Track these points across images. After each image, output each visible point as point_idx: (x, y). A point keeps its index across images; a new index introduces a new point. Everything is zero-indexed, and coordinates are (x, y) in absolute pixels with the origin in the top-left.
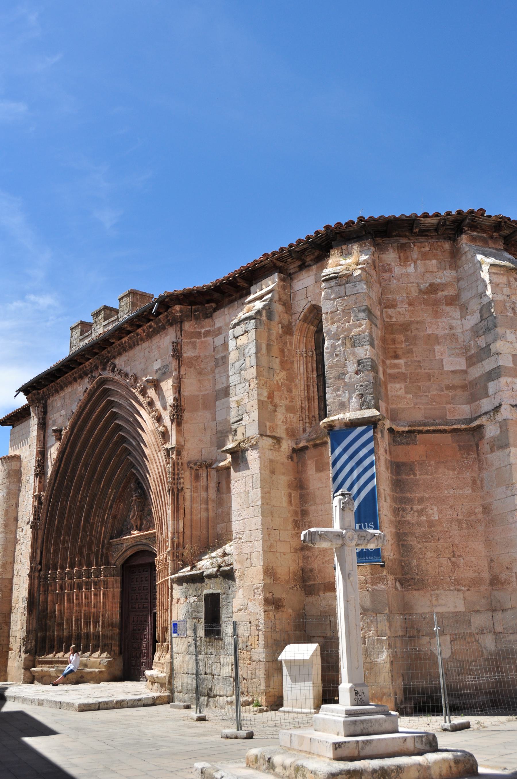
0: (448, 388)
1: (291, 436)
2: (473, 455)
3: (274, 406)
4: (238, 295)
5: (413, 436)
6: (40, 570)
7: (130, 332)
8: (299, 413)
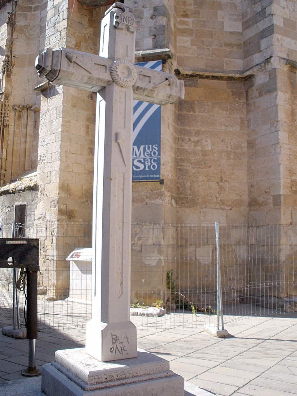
0: (227, 45)
5: (195, 79)
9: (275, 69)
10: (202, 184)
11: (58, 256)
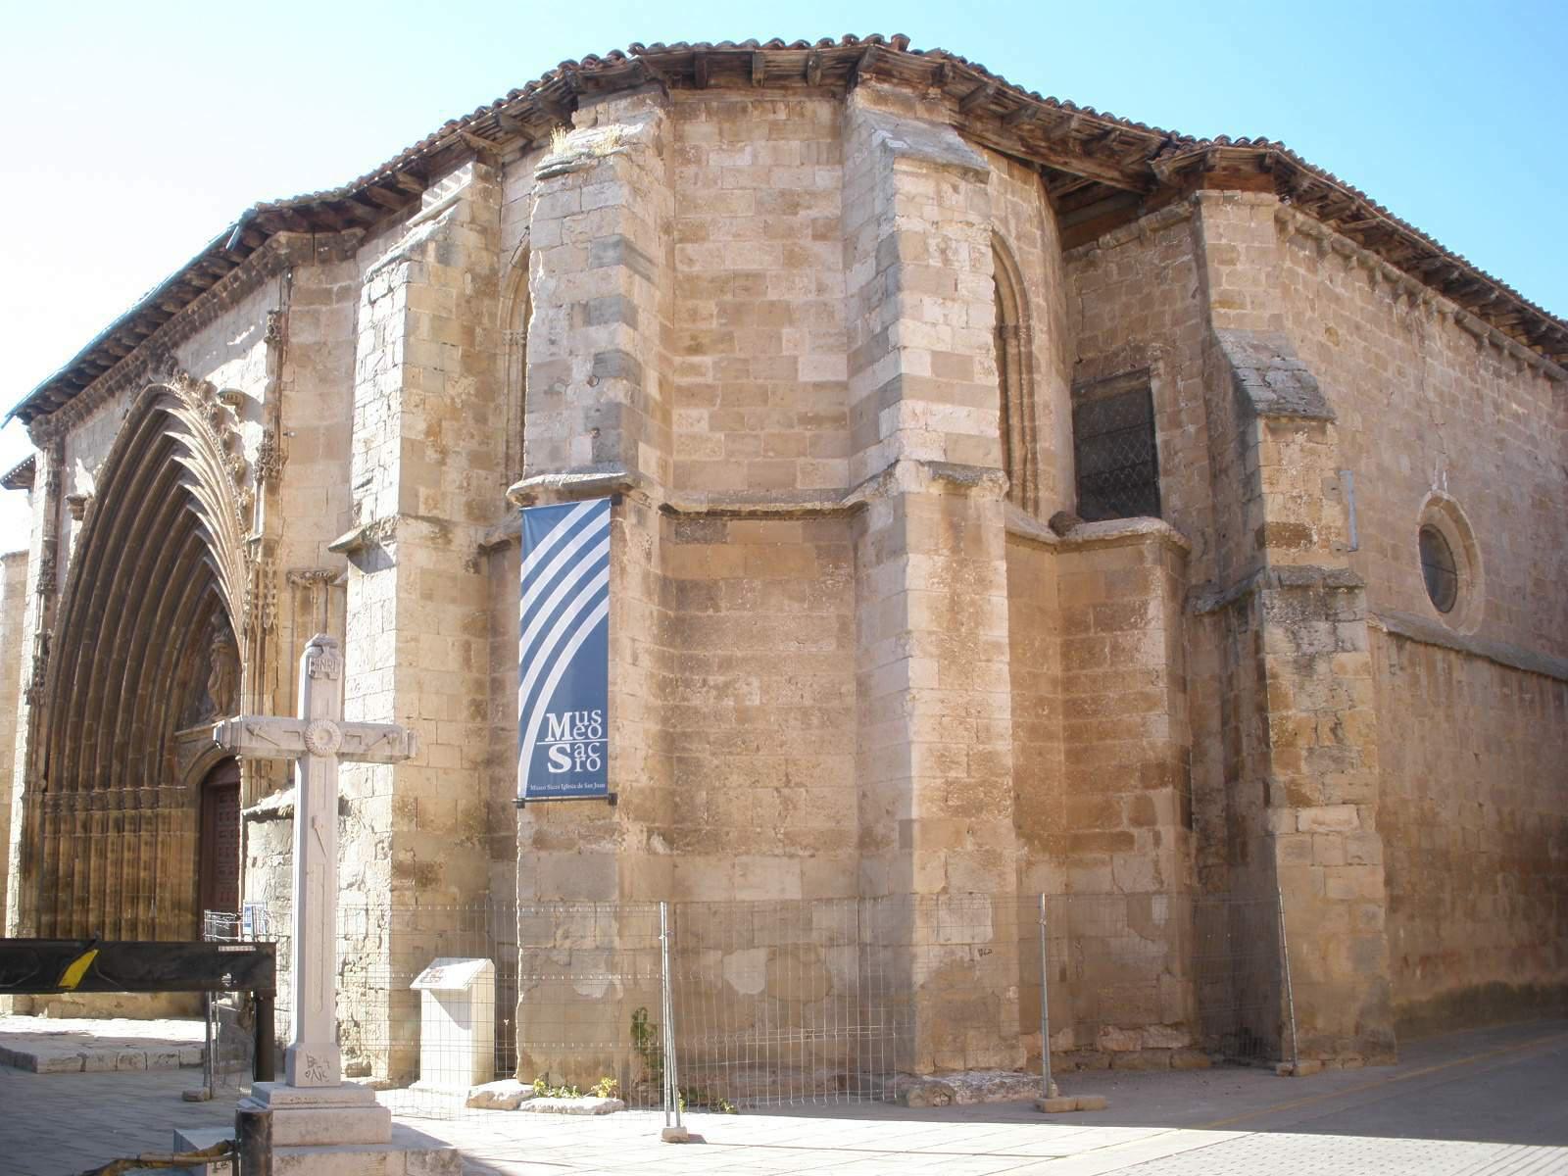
0: (805, 420)
1: (477, 519)
2: (846, 569)
3: (441, 452)
4: (405, 210)
5: (719, 523)
6: (45, 790)
7: (200, 290)
8: (501, 469)
9: (903, 494)
10: (737, 793)
11: (393, 981)
